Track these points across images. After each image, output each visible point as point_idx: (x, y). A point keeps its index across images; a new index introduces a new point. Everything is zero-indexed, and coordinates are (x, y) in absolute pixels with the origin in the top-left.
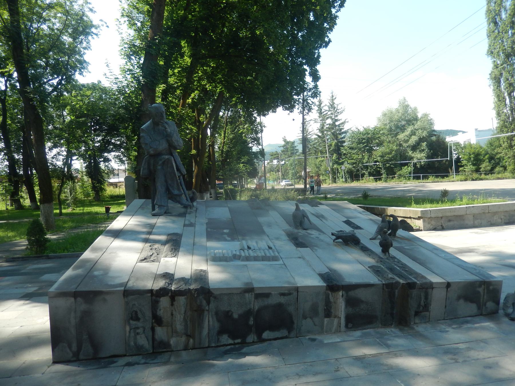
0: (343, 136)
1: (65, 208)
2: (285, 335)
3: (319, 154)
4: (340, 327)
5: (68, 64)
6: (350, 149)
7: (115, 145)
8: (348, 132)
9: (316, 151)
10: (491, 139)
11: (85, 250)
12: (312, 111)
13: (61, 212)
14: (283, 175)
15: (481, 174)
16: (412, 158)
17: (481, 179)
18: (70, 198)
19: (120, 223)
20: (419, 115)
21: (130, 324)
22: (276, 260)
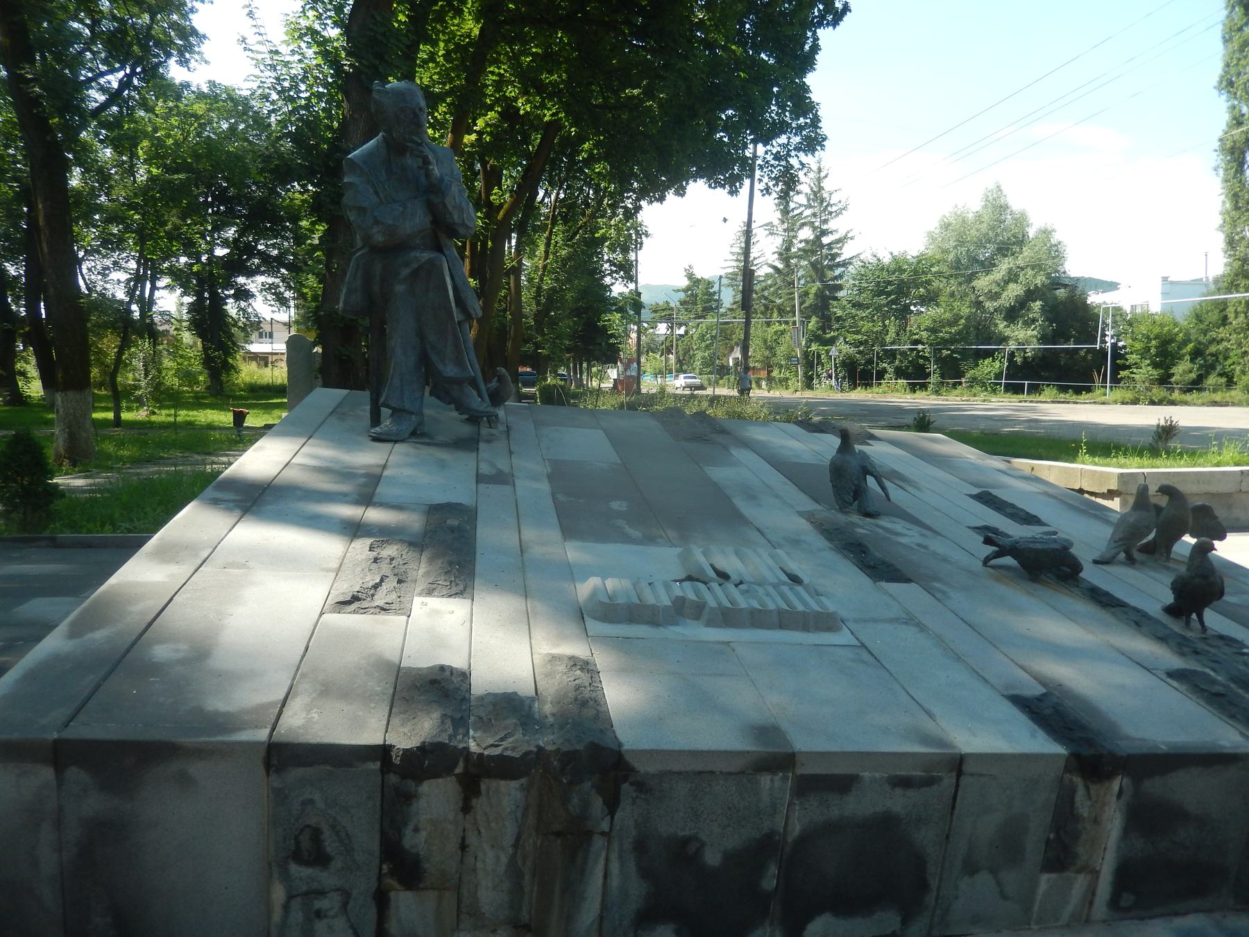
0: (838, 272)
1: (129, 409)
3: (775, 315)
4: (1091, 903)
5: (149, 36)
6: (854, 306)
7: (264, 256)
8: (850, 263)
9: (766, 307)
10: (1200, 303)
11: (130, 547)
13: (117, 416)
14: (679, 361)
15: (1172, 390)
16: (1004, 340)
17: (1173, 403)
18: (143, 384)
19: (262, 460)
20: (1031, 233)
21: (286, 877)
22: (829, 629)
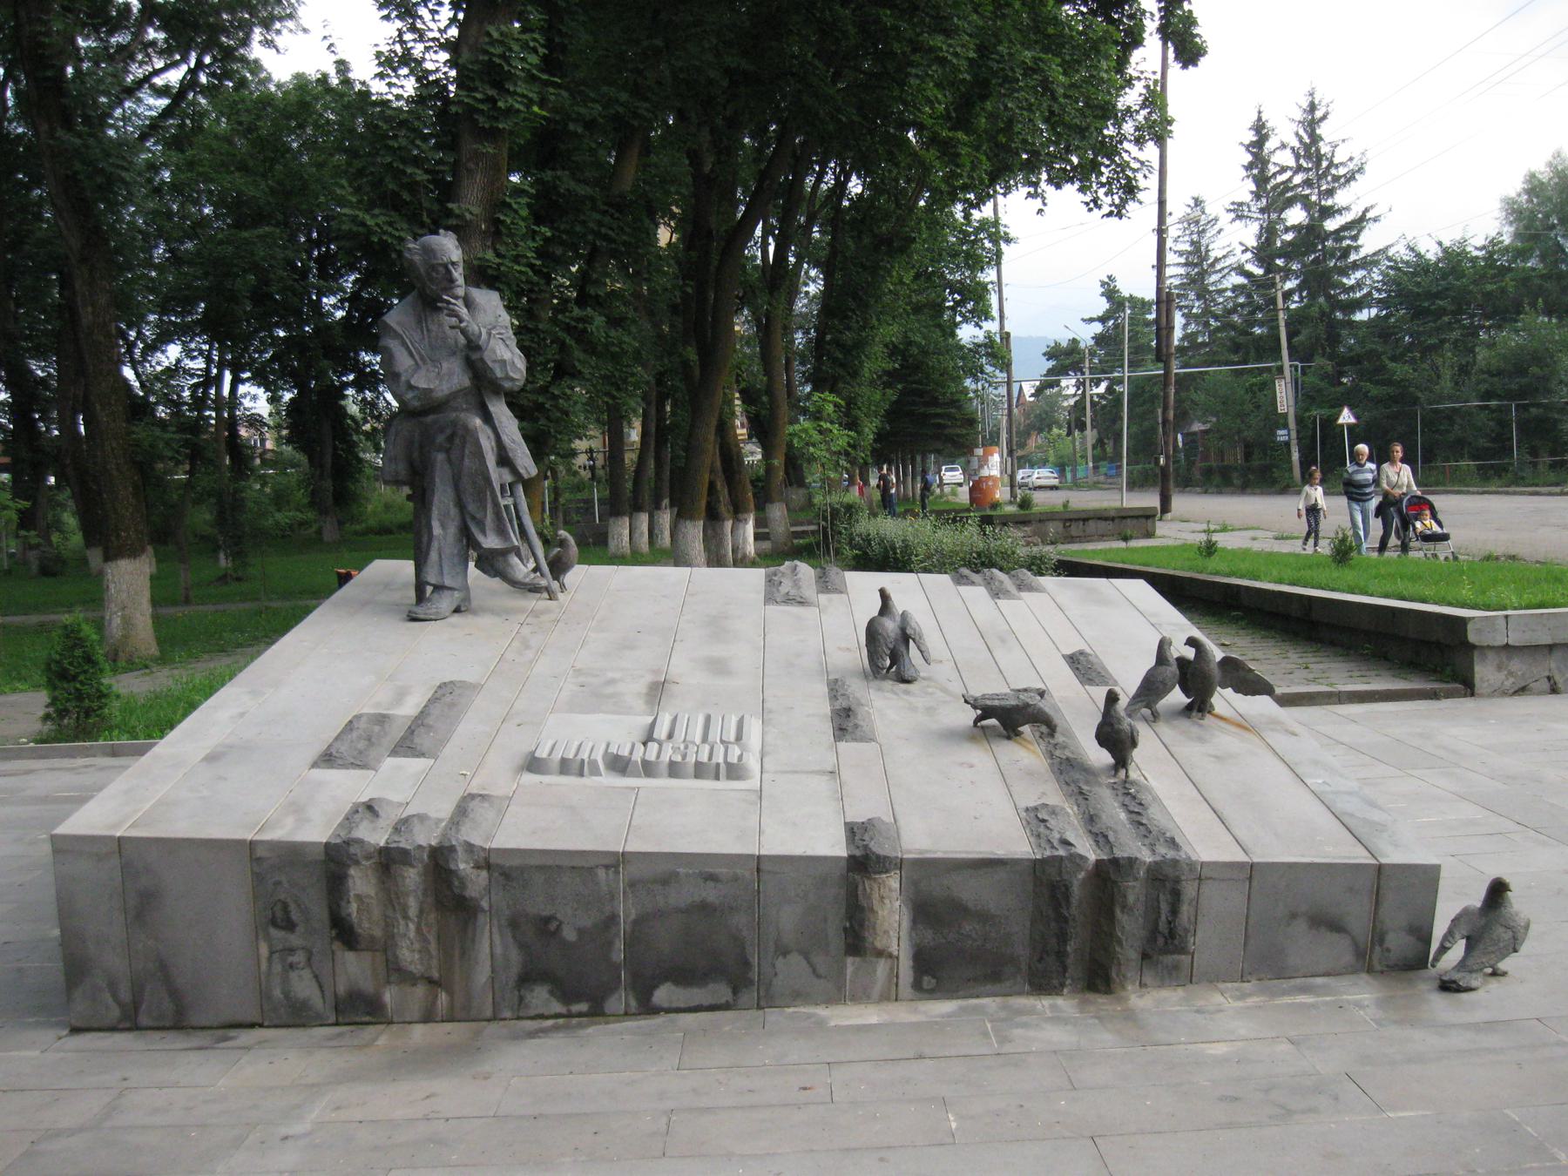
2: (723, 1001)
12: (1140, 196)
21: (268, 938)
